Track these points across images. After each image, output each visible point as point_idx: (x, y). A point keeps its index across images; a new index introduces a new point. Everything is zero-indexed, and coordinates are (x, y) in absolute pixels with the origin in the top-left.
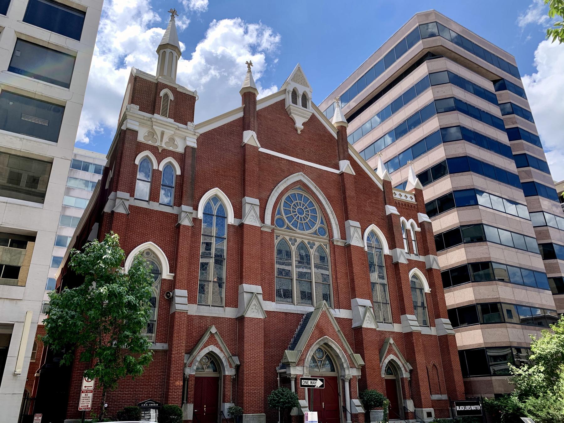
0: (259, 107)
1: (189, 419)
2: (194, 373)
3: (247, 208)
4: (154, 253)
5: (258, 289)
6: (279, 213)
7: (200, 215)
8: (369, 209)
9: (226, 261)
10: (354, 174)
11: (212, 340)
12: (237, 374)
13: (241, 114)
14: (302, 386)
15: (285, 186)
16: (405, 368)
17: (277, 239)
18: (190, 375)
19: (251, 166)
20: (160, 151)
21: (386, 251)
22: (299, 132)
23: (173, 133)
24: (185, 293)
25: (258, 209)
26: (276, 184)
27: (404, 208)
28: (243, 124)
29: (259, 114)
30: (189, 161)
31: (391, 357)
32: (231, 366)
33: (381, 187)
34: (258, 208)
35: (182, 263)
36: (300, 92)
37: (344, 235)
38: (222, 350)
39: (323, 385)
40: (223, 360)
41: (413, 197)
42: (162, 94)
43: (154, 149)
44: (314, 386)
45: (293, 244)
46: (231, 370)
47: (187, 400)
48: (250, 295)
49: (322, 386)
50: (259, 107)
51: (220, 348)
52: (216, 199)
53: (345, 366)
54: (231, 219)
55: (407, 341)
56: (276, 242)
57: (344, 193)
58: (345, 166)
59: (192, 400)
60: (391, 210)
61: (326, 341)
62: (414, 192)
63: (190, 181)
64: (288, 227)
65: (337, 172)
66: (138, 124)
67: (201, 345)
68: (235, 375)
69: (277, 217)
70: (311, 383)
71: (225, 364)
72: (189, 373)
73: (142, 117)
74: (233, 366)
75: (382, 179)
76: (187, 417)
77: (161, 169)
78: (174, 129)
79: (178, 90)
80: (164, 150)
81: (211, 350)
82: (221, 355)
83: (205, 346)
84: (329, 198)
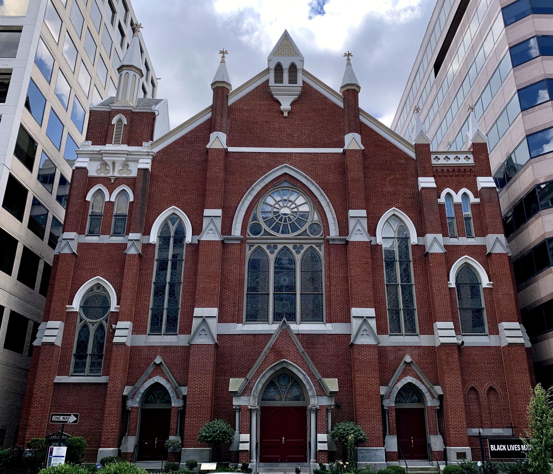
0: (231, 101)
1: (129, 451)
2: (393, 405)
3: (352, 223)
4: (103, 287)
5: (214, 311)
6: (255, 218)
7: (153, 238)
8: (388, 188)
9: (414, 287)
10: (363, 148)
11: (408, 369)
12: (441, 406)
13: (209, 115)
14: (52, 421)
15: (263, 185)
16: (431, 393)
17: (250, 249)
18: (132, 408)
19: (216, 171)
20: (112, 182)
21: (414, 239)
22: (286, 114)
23: (124, 159)
24: (128, 324)
25: (365, 222)
26: (249, 185)
27: (451, 176)
28: (209, 127)
29: (231, 110)
30: (139, 185)
31: (409, 379)
32: (178, 397)
33: (413, 155)
34: (366, 220)
35: (127, 293)
36: (286, 66)
37: (344, 229)
38: (168, 381)
39: (77, 420)
40: (170, 391)
41: (471, 156)
42: (114, 121)
43: (106, 181)
44: (66, 422)
45: (272, 252)
46: (179, 402)
47: (389, 432)
48: (360, 321)
49: (76, 421)
50: (231, 101)
51: (421, 380)
52: (173, 218)
53: (310, 393)
54: (189, 238)
55: (432, 360)
56: (248, 253)
57: (205, 170)
58: (353, 141)
59: (395, 431)
60: (426, 182)
61: (284, 365)
62: (472, 150)
63: (140, 206)
64: (266, 233)
65: (340, 150)
66: (87, 160)
67: (144, 377)
68: (439, 406)
69: (250, 223)
70: (64, 418)
71: (172, 395)
72: (131, 405)
73: (92, 152)
74: (436, 396)
75: (413, 143)
76: (127, 449)
77: (113, 199)
78: (125, 156)
79: (134, 111)
80: (117, 179)
81: (156, 381)
82: (168, 386)
83: (150, 377)
84: (325, 187)
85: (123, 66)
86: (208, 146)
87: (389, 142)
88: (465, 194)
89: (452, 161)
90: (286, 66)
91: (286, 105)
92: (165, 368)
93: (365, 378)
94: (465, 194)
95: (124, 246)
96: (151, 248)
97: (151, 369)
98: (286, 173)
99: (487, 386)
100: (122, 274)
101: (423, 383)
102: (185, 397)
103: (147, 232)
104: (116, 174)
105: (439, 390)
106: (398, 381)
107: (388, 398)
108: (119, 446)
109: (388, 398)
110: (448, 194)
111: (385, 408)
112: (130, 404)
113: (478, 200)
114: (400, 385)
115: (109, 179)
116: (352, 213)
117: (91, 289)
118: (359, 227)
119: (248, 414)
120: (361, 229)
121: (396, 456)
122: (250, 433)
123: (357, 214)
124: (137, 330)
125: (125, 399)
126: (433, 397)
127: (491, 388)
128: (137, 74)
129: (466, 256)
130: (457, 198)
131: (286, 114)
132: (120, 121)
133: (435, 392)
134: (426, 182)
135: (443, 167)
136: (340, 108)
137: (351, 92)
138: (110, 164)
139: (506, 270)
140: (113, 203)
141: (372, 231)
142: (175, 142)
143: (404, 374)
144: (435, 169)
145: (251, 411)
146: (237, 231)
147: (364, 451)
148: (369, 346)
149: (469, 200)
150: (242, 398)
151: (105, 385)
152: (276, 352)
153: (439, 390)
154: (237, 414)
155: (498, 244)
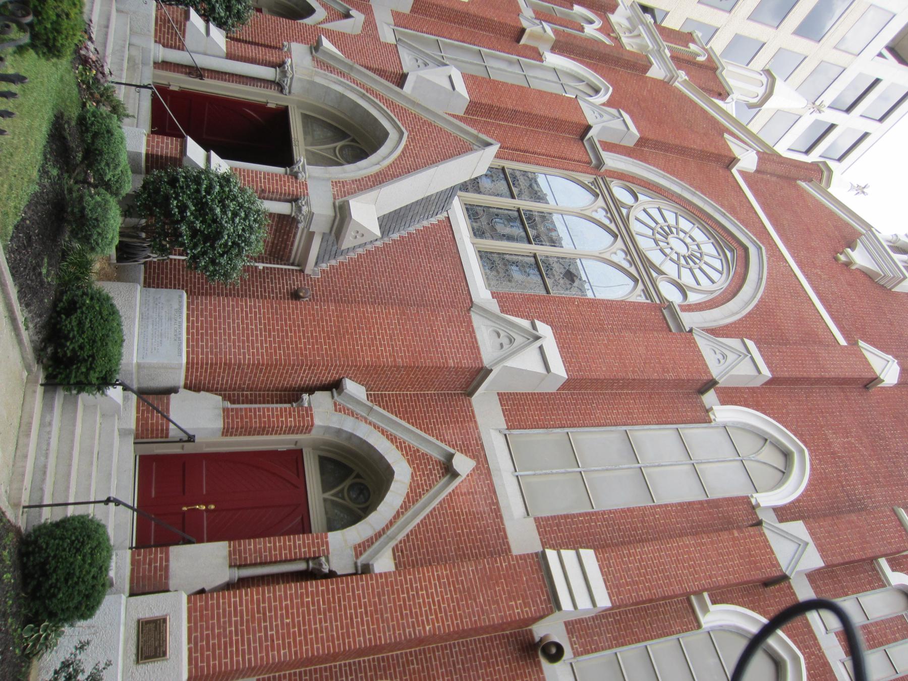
16: (370, 542)
31: (402, 473)
51: (405, 507)
61: (393, 135)
74: (361, 560)
85: (773, 80)
92: (444, 491)
97: (432, 446)
102: (366, 569)
103: (553, 50)
105: (384, 563)
106: (392, 439)
107: (338, 408)
111: (305, 396)
112: (320, 405)
120: (515, 344)
125: (335, 386)
126: (360, 549)
133: (377, 552)
138: (635, 33)
141: (730, 396)
143: (414, 457)
147: (176, 306)
153: (384, 563)
154: (280, 170)
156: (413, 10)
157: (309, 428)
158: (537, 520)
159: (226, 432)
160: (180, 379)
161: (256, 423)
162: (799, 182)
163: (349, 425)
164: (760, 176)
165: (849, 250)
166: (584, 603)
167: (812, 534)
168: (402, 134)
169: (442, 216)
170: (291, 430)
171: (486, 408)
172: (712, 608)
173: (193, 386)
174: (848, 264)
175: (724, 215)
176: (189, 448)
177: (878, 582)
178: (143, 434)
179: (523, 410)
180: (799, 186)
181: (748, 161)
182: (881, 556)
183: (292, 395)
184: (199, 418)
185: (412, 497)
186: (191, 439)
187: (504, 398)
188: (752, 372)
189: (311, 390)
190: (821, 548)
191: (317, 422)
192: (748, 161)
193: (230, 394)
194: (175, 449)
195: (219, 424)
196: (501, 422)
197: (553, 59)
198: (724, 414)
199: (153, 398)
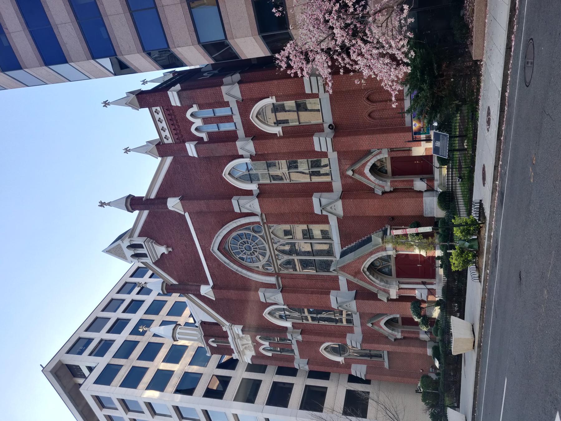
15: (232, 264)
22: (170, 249)
23: (239, 340)
31: (367, 171)
58: (174, 204)
61: (366, 270)
67: (381, 331)
75: (160, 159)
86: (214, 299)
87: (165, 176)
88: (192, 115)
89: (164, 124)
90: (132, 252)
91: (162, 250)
93: (370, 208)
94: (192, 115)
95: (297, 342)
96: (295, 325)
98: (218, 249)
99: (366, 103)
100: (316, 342)
101: (369, 161)
103: (286, 328)
104: (250, 342)
106: (369, 179)
107: (383, 187)
108: (426, 341)
109: (383, 187)
110: (197, 129)
112: (388, 188)
113: (195, 106)
114: (372, 178)
115: (254, 346)
116: (237, 210)
117: (328, 352)
118: (248, 206)
119: (401, 290)
121: (430, 184)
122: (415, 289)
123: (237, 204)
124: (352, 331)
125: (384, 193)
126: (380, 153)
127: (368, 99)
128: (177, 332)
129: (250, 118)
130: (198, 122)
131: (170, 249)
132: (213, 341)
134: (191, 149)
135: (171, 132)
136: (149, 215)
137: (133, 203)
138: (244, 346)
139: (255, 87)
140: (260, 186)
141: (249, 193)
142: (218, 313)
144: (177, 141)
145: (399, 289)
146: (272, 280)
148: (343, 205)
149: (196, 112)
150: (391, 294)
151: (388, 352)
152: (356, 274)
155: (232, 93)
156: (346, 335)
157: (391, 182)
158: (327, 157)
159: (412, 181)
160: (424, 194)
161: (405, 183)
162: (177, 283)
163: (381, 183)
164: (198, 284)
165: (166, 253)
166: (322, 139)
167: (237, 151)
168: (363, 270)
169: (344, 249)
170: (396, 181)
171: (337, 186)
172: (278, 133)
173: (421, 192)
174: (168, 247)
175: (225, 262)
176: (421, 176)
177: (209, 134)
178: (432, 180)
179: (327, 188)
180: (177, 282)
181: (206, 290)
182: (206, 143)
183: (395, 190)
184: (420, 185)
185: (364, 165)
186: (421, 179)
187: (331, 191)
188: (241, 202)
189: (391, 192)
190: (235, 146)
191: (389, 183)
192: (206, 290)
193: (418, 339)
194: (425, 176)
195: (414, 183)
196: (334, 184)
197: (288, 324)
198: (253, 187)
199: (430, 189)
